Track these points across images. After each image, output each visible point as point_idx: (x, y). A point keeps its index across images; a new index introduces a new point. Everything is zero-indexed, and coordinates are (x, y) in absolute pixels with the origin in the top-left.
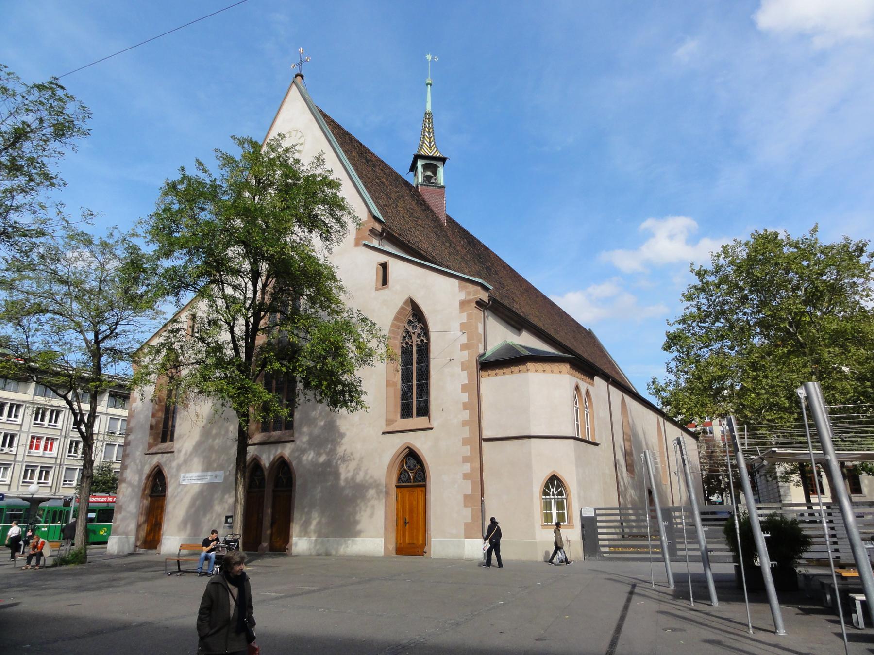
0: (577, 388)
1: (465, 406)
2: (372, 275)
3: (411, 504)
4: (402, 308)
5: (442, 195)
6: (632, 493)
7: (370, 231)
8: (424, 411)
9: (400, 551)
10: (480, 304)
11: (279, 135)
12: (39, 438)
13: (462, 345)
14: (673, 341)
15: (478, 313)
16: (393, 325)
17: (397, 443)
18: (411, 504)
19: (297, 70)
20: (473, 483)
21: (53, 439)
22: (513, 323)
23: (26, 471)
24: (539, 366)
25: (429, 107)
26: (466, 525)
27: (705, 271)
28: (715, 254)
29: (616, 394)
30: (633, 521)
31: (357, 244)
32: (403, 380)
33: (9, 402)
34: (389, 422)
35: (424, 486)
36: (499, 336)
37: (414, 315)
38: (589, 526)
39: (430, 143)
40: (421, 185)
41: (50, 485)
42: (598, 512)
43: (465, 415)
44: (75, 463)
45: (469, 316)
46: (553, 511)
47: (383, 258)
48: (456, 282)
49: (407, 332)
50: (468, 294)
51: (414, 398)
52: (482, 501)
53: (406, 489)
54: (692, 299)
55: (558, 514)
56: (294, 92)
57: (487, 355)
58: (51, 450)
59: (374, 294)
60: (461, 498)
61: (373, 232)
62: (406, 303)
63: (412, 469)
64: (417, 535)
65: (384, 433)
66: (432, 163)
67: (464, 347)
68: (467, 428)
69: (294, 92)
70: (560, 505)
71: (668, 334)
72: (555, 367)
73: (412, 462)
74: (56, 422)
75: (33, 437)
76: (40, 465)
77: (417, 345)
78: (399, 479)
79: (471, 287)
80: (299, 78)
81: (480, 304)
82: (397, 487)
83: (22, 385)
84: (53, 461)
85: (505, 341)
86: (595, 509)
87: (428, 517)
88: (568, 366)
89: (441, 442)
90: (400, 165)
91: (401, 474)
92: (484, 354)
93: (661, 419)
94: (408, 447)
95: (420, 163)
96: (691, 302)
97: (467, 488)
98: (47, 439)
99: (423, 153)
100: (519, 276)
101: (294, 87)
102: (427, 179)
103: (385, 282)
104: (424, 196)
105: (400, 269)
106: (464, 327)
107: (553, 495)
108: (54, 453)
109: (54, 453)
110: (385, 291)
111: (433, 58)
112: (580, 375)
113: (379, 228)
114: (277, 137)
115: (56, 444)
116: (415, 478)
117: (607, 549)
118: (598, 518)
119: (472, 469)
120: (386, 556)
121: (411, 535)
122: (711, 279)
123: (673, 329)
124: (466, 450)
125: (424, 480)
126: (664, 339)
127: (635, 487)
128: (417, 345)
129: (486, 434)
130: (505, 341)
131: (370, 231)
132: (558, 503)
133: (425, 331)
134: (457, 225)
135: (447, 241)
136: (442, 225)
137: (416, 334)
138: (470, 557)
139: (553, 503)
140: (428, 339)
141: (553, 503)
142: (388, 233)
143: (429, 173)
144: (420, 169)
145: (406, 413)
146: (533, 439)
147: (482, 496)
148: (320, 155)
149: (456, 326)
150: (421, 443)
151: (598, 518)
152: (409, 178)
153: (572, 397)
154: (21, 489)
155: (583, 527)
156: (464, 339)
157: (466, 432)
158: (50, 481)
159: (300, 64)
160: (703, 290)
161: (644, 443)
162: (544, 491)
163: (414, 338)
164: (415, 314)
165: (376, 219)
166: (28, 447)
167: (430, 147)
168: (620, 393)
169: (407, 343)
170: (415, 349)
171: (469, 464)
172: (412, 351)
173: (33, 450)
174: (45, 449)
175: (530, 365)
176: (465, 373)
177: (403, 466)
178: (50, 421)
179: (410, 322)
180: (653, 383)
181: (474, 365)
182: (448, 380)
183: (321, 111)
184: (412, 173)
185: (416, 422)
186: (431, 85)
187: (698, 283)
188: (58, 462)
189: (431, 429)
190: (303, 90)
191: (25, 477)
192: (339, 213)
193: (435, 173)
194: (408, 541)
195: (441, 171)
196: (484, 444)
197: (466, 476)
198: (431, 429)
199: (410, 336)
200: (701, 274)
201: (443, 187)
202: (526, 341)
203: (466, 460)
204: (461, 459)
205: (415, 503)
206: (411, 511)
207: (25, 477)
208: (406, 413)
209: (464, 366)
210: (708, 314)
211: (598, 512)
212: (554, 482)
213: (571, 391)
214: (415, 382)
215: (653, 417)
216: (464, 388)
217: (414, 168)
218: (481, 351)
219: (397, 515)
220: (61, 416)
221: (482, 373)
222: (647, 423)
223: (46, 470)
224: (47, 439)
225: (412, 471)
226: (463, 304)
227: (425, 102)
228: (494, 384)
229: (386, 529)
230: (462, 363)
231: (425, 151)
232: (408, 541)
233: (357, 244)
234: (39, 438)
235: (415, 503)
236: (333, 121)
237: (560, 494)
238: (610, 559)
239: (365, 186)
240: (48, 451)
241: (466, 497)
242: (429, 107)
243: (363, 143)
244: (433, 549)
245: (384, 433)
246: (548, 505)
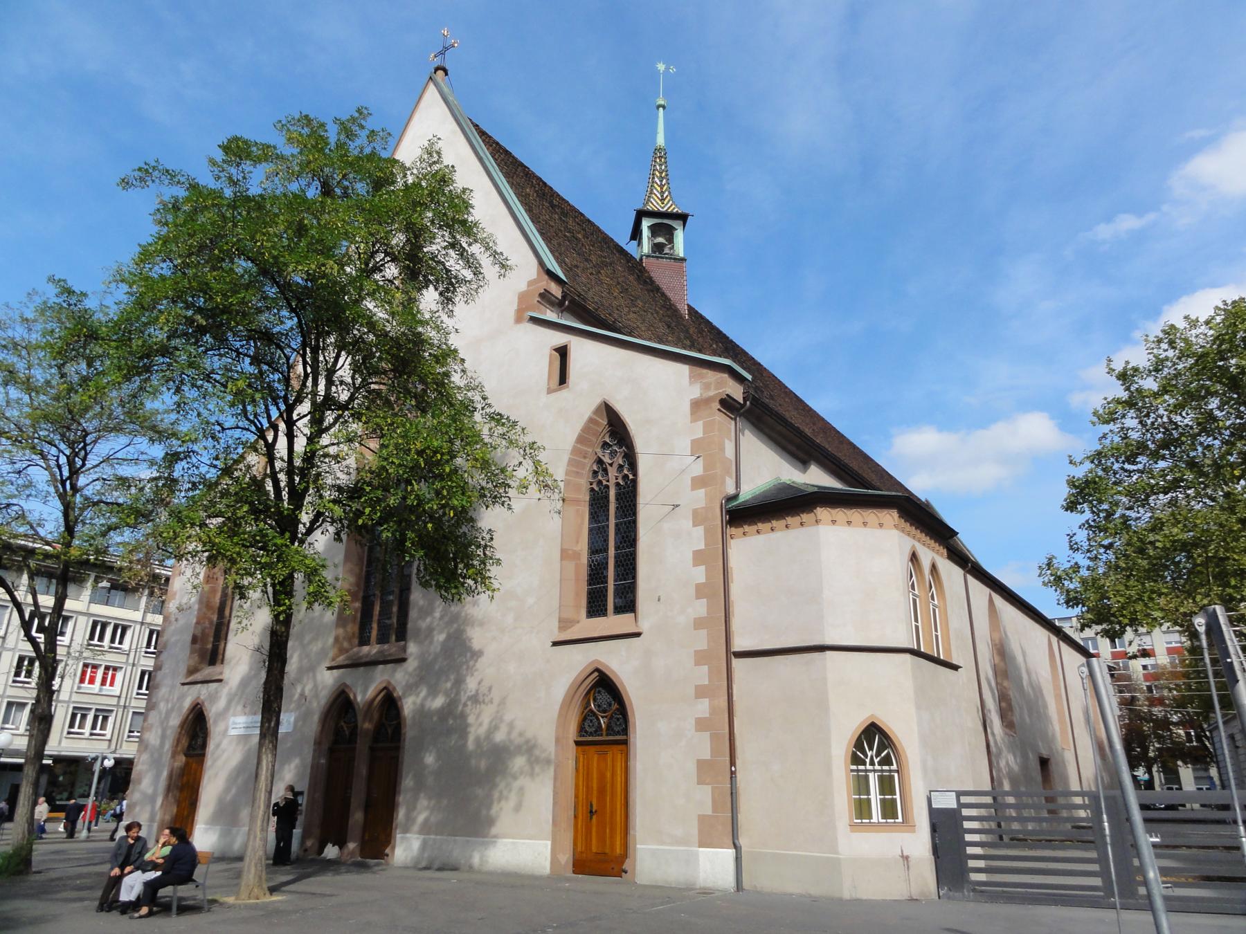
0: (914, 558)
1: (700, 591)
2: (541, 366)
3: (602, 777)
4: (591, 420)
5: (681, 273)
6: (1009, 761)
7: (541, 295)
8: (628, 604)
9: (582, 866)
10: (727, 404)
11: (359, 111)
12: (95, 667)
13: (693, 479)
14: (1083, 493)
15: (726, 424)
16: (575, 451)
17: (579, 660)
18: (602, 777)
19: (438, 62)
20: (714, 738)
21: (115, 669)
22: (793, 449)
23: (74, 716)
24: (840, 514)
25: (661, 140)
26: (702, 819)
27: (1136, 370)
28: (1151, 338)
29: (979, 591)
30: (1010, 806)
31: (518, 320)
32: (593, 551)
33: (113, 622)
34: (564, 624)
35: (625, 743)
36: (764, 468)
37: (613, 434)
38: (945, 827)
39: (662, 193)
40: (648, 256)
41: (108, 737)
42: (964, 800)
43: (700, 608)
44: (22, 693)
45: (708, 428)
46: (872, 797)
47: (560, 338)
48: (684, 369)
49: (600, 462)
50: (706, 387)
51: (610, 581)
52: (733, 773)
53: (592, 749)
54: (1114, 420)
55: (883, 802)
56: (432, 92)
57: (742, 499)
58: (112, 684)
59: (545, 398)
60: (692, 767)
61: (545, 297)
62: (597, 411)
63: (604, 711)
64: (612, 837)
65: (555, 644)
66: (666, 222)
67: (698, 482)
68: (703, 633)
69: (432, 92)
70: (886, 785)
71: (1072, 483)
72: (871, 515)
73: (604, 697)
74: (120, 643)
75: (86, 666)
76: (94, 707)
77: (618, 484)
78: (582, 730)
79: (711, 376)
80: (440, 73)
81: (727, 404)
82: (577, 743)
83: (130, 599)
84: (114, 701)
85: (778, 478)
86: (959, 794)
87: (631, 803)
88: (895, 514)
89: (655, 662)
90: (618, 230)
91: (584, 719)
92: (735, 497)
93: (1054, 639)
94: (597, 670)
95: (646, 223)
96: (1111, 426)
97: (703, 747)
98: (107, 668)
99: (650, 207)
100: (811, 409)
101: (432, 87)
102: (658, 248)
103: (563, 379)
104: (652, 274)
105: (589, 355)
106: (698, 448)
107: (872, 763)
108: (116, 690)
109: (116, 690)
110: (564, 393)
111: (667, 68)
112: (918, 533)
113: (556, 291)
114: (357, 115)
115: (119, 676)
116: (609, 727)
117: (981, 864)
118: (965, 812)
119: (713, 711)
120: (554, 877)
121: (600, 836)
122: (1150, 384)
123: (1080, 472)
124: (702, 675)
125: (625, 731)
126: (1065, 491)
127: (1012, 748)
128: (618, 484)
129: (739, 644)
130: (778, 478)
131: (541, 295)
132: (881, 779)
133: (631, 460)
134: (708, 323)
135: (686, 338)
136: (682, 317)
137: (616, 466)
138: (710, 884)
139: (873, 780)
140: (635, 474)
141: (873, 780)
142: (572, 301)
143: (660, 240)
144: (646, 232)
145: (596, 607)
146: (828, 653)
147: (733, 762)
148: (431, 144)
149: (684, 445)
150: (620, 661)
151: (965, 812)
152: (631, 248)
153: (906, 575)
154: (65, 743)
155: (934, 829)
156: (698, 469)
157: (701, 641)
158: (108, 732)
159: (442, 53)
160: (1130, 404)
161: (1025, 676)
162: (854, 754)
163: (612, 472)
164: (614, 431)
165: (551, 274)
166: (77, 680)
167: (662, 200)
168: (987, 590)
169: (600, 482)
170: (612, 493)
171: (706, 701)
172: (607, 497)
173: (86, 684)
174: (103, 682)
175: (822, 513)
176: (700, 531)
177: (588, 704)
178: (113, 641)
179: (605, 445)
180: (1049, 565)
181: (717, 518)
182: (670, 545)
183: (476, 126)
184: (635, 243)
185: (613, 622)
186: (664, 107)
187: (1124, 395)
188: (122, 703)
189: (638, 635)
190: (446, 90)
191: (72, 725)
192: (464, 242)
193: (671, 240)
194: (594, 849)
195: (679, 236)
196: (736, 662)
197: (701, 725)
198: (638, 635)
199: (605, 470)
200: (1125, 377)
201: (683, 260)
202: (816, 477)
203: (701, 692)
204: (692, 691)
205: (609, 774)
206: (602, 791)
207: (72, 725)
208: (596, 607)
209: (698, 518)
210: (1142, 447)
211: (964, 800)
212: (874, 737)
213: (900, 564)
214: (612, 552)
215: (1040, 635)
216: (699, 558)
217: (636, 234)
218: (731, 490)
219: (576, 796)
220: (129, 633)
221: (733, 531)
222: (1031, 643)
223: (103, 715)
224: (107, 668)
225: (603, 715)
226: (697, 405)
227: (655, 133)
228: (752, 549)
229: (555, 823)
230: (695, 513)
231: (655, 205)
232: (594, 849)
233: (518, 320)
234: (95, 667)
235: (609, 774)
236: (507, 153)
237: (886, 761)
238: (994, 898)
239: (542, 234)
240: (107, 687)
241: (701, 764)
242: (661, 140)
243: (549, 183)
244: (638, 868)
245: (555, 644)
246: (861, 784)
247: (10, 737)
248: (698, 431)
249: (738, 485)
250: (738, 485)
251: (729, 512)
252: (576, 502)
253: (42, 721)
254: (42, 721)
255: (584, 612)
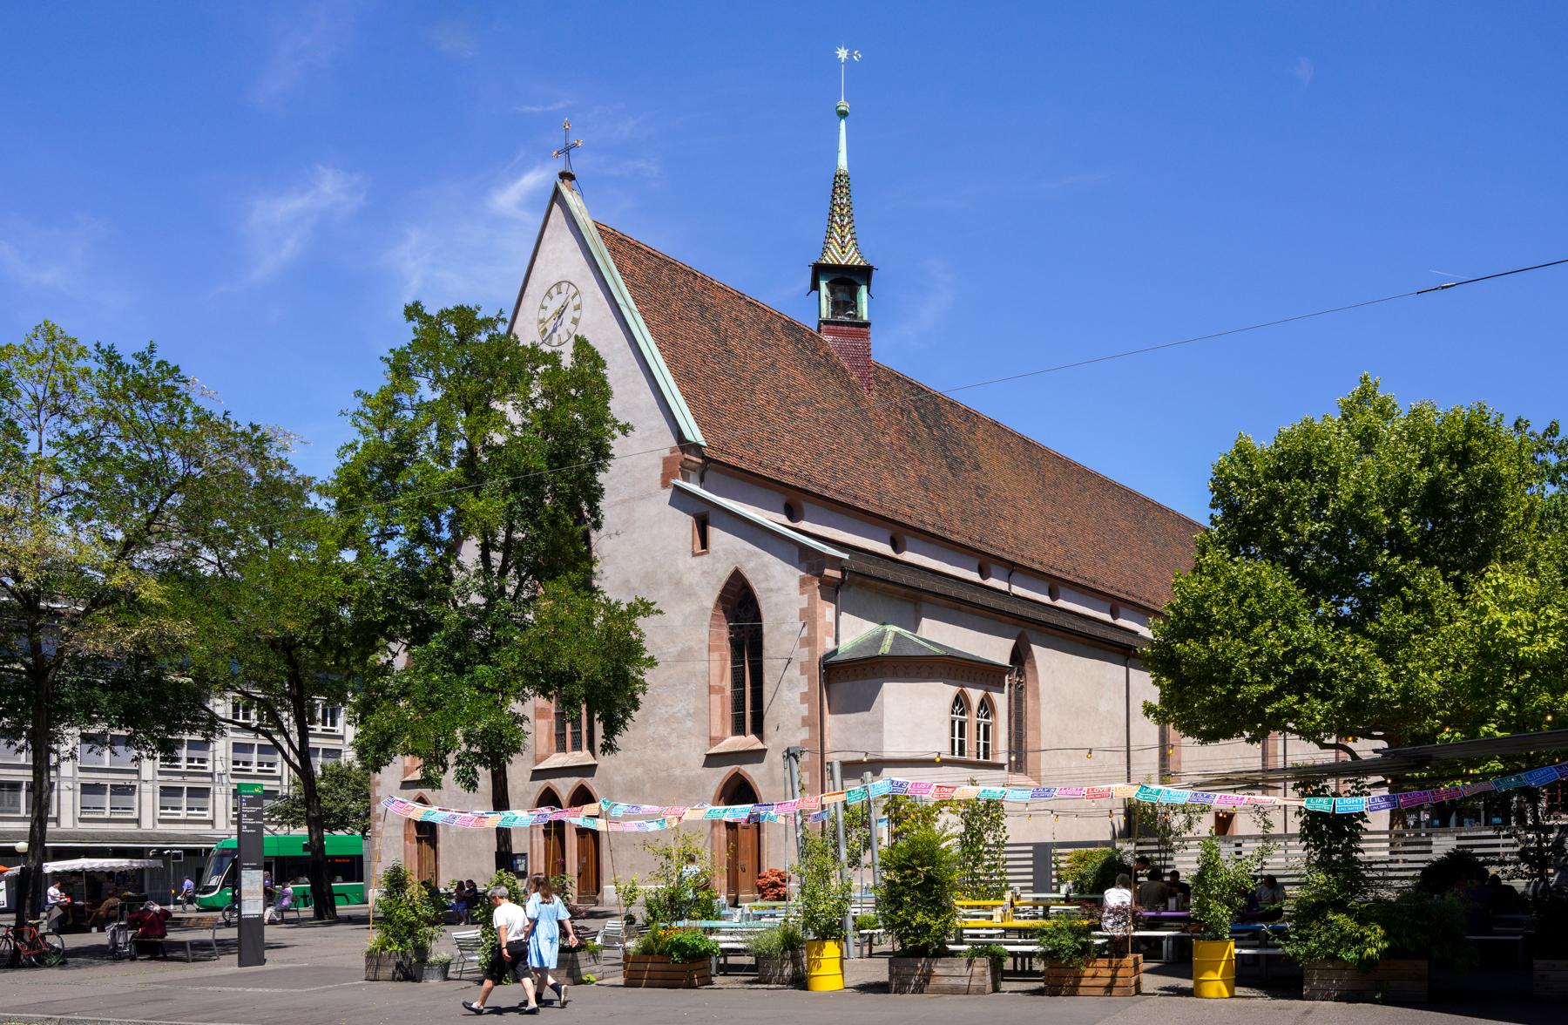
25: (843, 162)
45: (812, 599)
66: (847, 281)
92: (835, 652)
105: (540, 840)
111: (850, 55)
201: (867, 325)
218: (830, 645)
231: (834, 256)
247: (14, 827)
248: (804, 601)
249: (837, 641)
250: (837, 641)
251: (826, 666)
252: (719, 648)
253: (1291, 837)
254: (1291, 837)
255: (729, 731)
